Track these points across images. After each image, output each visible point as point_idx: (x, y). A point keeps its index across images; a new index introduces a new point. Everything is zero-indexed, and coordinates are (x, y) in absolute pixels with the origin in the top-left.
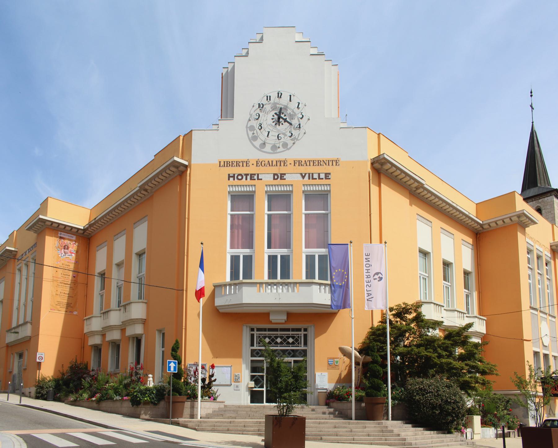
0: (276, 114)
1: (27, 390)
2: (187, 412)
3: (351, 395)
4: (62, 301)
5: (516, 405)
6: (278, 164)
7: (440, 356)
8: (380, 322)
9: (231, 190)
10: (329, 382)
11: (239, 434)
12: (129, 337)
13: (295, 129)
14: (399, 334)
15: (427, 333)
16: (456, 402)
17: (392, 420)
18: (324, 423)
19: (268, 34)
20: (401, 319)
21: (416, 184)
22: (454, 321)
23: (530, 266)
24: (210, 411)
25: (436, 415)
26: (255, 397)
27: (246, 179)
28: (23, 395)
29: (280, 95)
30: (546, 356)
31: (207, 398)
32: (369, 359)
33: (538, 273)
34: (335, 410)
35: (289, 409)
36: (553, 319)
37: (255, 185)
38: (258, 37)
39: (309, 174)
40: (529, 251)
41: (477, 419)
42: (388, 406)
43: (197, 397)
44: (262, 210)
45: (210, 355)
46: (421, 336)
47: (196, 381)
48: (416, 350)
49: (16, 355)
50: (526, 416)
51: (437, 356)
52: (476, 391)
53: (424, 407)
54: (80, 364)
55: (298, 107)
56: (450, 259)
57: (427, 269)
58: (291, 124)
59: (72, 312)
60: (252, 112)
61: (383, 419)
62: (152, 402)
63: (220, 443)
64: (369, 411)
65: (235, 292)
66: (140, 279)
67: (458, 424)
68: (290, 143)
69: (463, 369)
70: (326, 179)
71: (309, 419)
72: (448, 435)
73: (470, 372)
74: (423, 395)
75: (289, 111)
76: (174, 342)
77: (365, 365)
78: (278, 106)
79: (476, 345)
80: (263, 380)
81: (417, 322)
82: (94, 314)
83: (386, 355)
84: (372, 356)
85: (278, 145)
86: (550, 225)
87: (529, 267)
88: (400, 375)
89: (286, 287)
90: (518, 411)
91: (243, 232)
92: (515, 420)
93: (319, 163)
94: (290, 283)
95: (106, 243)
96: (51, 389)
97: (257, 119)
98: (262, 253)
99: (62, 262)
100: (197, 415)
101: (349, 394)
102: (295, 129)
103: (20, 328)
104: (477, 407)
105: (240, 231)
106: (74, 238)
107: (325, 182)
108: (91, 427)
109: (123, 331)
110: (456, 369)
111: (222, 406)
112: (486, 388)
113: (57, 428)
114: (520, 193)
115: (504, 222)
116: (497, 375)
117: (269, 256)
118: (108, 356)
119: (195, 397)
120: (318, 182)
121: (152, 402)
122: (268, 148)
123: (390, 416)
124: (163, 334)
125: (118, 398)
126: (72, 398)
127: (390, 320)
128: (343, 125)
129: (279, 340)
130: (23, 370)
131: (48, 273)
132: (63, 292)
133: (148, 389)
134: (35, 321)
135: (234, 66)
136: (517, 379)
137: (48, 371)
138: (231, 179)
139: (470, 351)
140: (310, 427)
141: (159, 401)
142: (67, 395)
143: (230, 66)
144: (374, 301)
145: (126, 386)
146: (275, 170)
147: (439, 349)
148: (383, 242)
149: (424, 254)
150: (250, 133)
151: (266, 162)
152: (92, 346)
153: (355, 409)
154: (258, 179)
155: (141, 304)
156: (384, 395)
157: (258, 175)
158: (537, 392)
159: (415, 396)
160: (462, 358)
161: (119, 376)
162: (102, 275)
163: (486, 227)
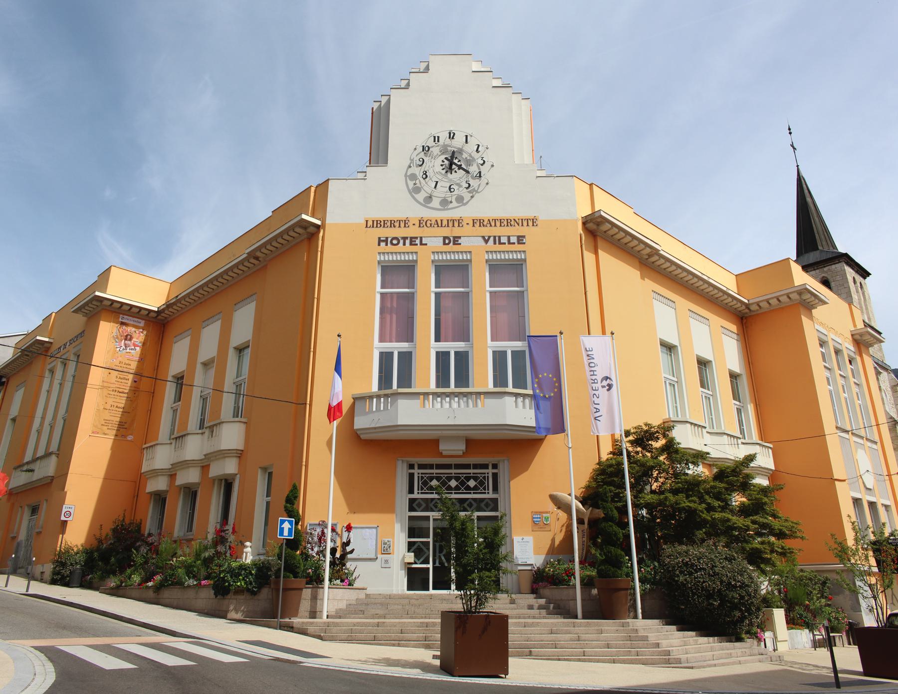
0: (446, 158)
1: (38, 569)
2: (305, 605)
3: (574, 574)
4: (112, 418)
5: (838, 589)
6: (451, 224)
7: (710, 509)
8: (611, 453)
9: (382, 259)
10: (536, 552)
11: (394, 645)
12: (213, 480)
13: (473, 178)
14: (642, 474)
15: (687, 471)
16: (743, 586)
17: (643, 618)
18: (532, 625)
19: (436, 63)
20: (643, 449)
21: (648, 250)
22: (728, 451)
23: (827, 365)
24: (342, 605)
25: (714, 609)
26: (416, 579)
27: (404, 244)
28: (30, 577)
29: (452, 136)
30: (872, 505)
31: (338, 581)
32: (600, 513)
33: (841, 375)
34: (549, 602)
35: (480, 601)
36: (874, 446)
37: (416, 253)
38: (423, 66)
39: (495, 237)
40: (822, 343)
41: (779, 615)
42: (634, 594)
43: (323, 580)
44: (427, 287)
45: (344, 508)
46: (676, 475)
47: (322, 552)
48: (672, 498)
49: (26, 509)
50: (857, 607)
51: (706, 509)
52: (774, 565)
53: (694, 594)
54: (130, 524)
55: (477, 150)
56: (707, 355)
57: (674, 369)
58: (467, 172)
59: (124, 436)
60: (414, 156)
61: (629, 617)
62: (248, 590)
63: (365, 662)
64: (604, 606)
65: (386, 408)
66: (238, 386)
67: (751, 624)
68: (467, 196)
69: (748, 530)
70: (519, 243)
71: (512, 618)
72: (737, 644)
73: (760, 535)
74: (691, 574)
75: (465, 156)
76: (291, 488)
77: (594, 523)
78: (449, 148)
79: (764, 491)
80: (429, 549)
81: (668, 454)
82: (160, 440)
83: (626, 506)
84: (604, 508)
85: (449, 199)
86: (847, 305)
87: (825, 367)
88: (649, 539)
89: (465, 399)
90: (842, 600)
91: (399, 316)
92: (840, 616)
93: (509, 222)
94: (471, 393)
95: (190, 332)
96: (78, 567)
97: (421, 166)
98: (427, 349)
99: (120, 359)
100: (321, 612)
101: (570, 573)
102: (474, 178)
103: (38, 462)
104: (776, 593)
105: (394, 317)
106: (142, 323)
107: (518, 247)
108: (155, 635)
109: (205, 468)
110: (739, 529)
111: (362, 595)
112: (787, 561)
113: (95, 635)
114: (795, 258)
115: (779, 301)
116: (802, 538)
117: (437, 353)
118: (177, 510)
119: (319, 580)
120: (507, 247)
121: (248, 590)
122: (436, 203)
123: (640, 611)
124: (270, 474)
125: (192, 582)
126: (112, 582)
127: (628, 453)
128: (539, 173)
129: (453, 483)
130: (36, 534)
131: (95, 376)
132: (116, 404)
133: (242, 567)
134: (64, 452)
135: (389, 99)
136: (836, 546)
137: (76, 535)
138: (383, 244)
139: (756, 499)
140: (515, 633)
141: (260, 587)
142: (102, 579)
143: (384, 100)
144: (603, 420)
145: (207, 562)
146: (446, 232)
147: (707, 497)
148: (608, 332)
149: (669, 348)
150: (411, 184)
151: (433, 222)
152: (151, 494)
153: (583, 600)
154: (421, 244)
155: (238, 424)
156: (627, 575)
157: (421, 238)
158: (870, 566)
159: (678, 576)
160: (744, 511)
161: (195, 545)
162: (179, 380)
163: (754, 308)
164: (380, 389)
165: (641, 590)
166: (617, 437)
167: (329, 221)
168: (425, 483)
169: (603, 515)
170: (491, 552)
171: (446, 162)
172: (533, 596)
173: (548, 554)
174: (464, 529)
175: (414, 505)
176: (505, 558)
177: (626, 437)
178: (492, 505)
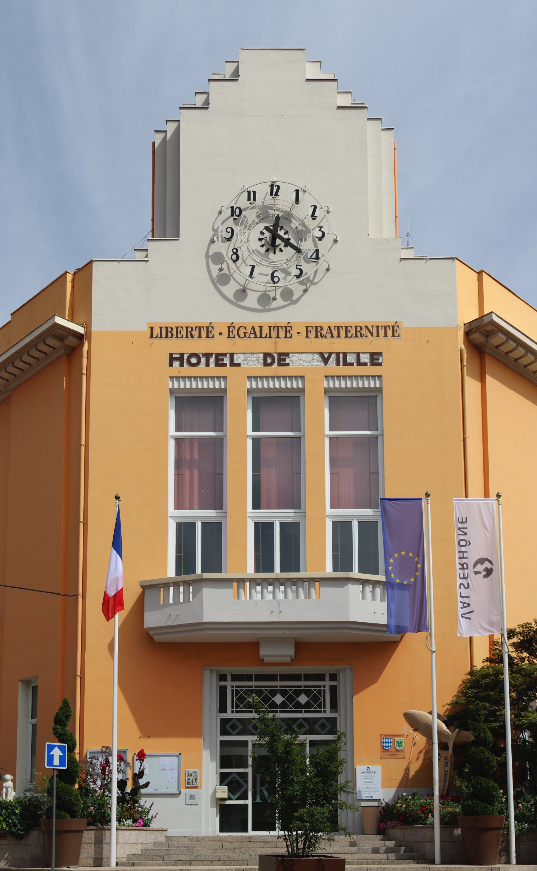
0: (267, 228)
2: (87, 851)
3: (432, 811)
8: (488, 660)
9: (176, 386)
10: (385, 784)
17: (518, 863)
19: (249, 62)
20: (530, 654)
24: (136, 850)
26: (231, 818)
27: (207, 364)
29: (275, 191)
31: (130, 822)
32: (469, 736)
34: (399, 844)
35: (310, 843)
37: (225, 378)
38: (229, 69)
39: (338, 354)
42: (508, 835)
43: (110, 821)
44: (241, 429)
47: (107, 787)
55: (313, 216)
61: (499, 862)
62: (12, 834)
65: (187, 600)
68: (297, 289)
70: (373, 364)
71: (351, 863)
75: (295, 224)
78: (271, 212)
80: (247, 782)
83: (504, 727)
84: (475, 729)
85: (272, 294)
89: (294, 588)
91: (202, 473)
93: (358, 331)
94: (302, 580)
98: (243, 519)
100: (109, 858)
101: (428, 810)
102: (308, 260)
105: (196, 473)
111: (161, 838)
117: (256, 525)
119: (105, 821)
120: (356, 370)
121: (12, 834)
122: (252, 300)
123: (514, 854)
128: (405, 254)
138: (176, 364)
141: (28, 829)
143: (171, 128)
150: (215, 269)
151: (249, 330)
153: (442, 842)
156: (501, 812)
157: (232, 355)
164: (178, 572)
165: (517, 830)
166: (497, 637)
167: (95, 328)
168: (241, 699)
169: (473, 738)
170: (324, 782)
171: (267, 234)
172: (379, 837)
173: (400, 786)
174: (287, 752)
175: (228, 727)
176: (342, 789)
177: (509, 638)
178: (329, 726)
